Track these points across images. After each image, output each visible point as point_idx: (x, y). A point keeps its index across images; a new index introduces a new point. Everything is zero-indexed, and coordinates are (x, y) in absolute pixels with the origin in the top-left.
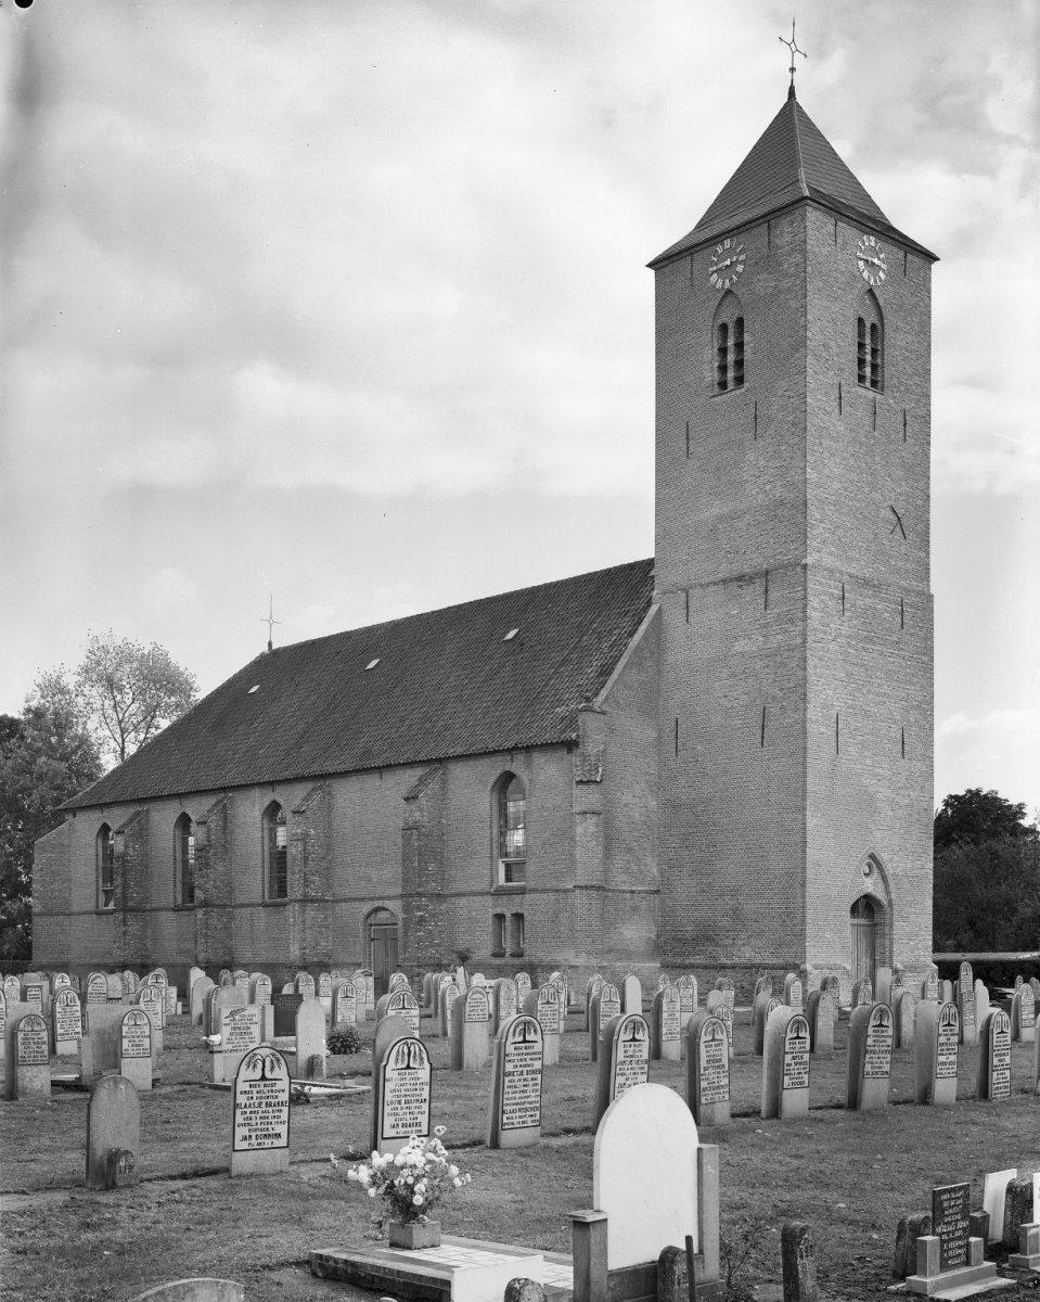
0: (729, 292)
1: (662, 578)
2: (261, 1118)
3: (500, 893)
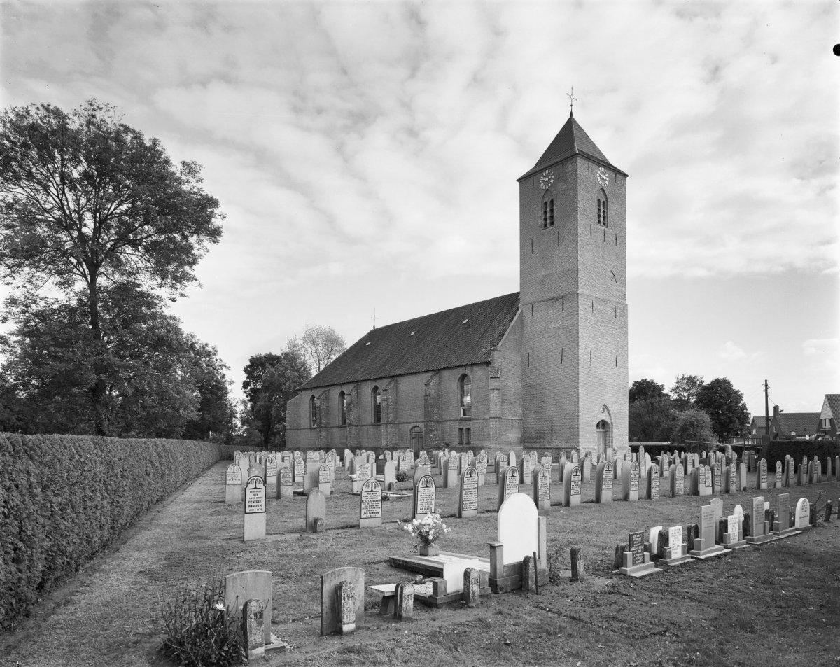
1: (523, 299)
3: (462, 420)
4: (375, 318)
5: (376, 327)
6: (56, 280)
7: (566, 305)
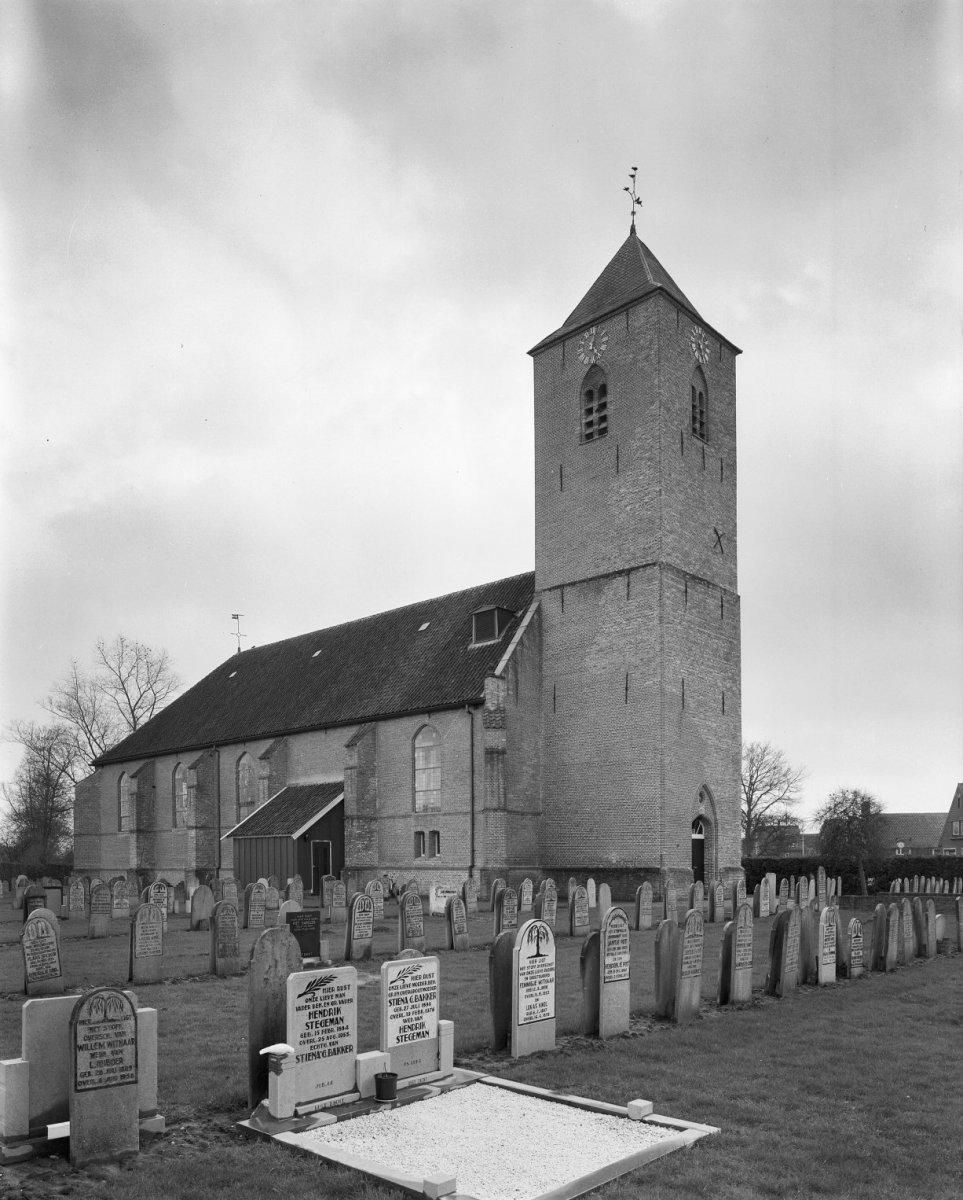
0: (594, 365)
2: (337, 995)
4: (239, 635)
5: (242, 651)
6: (238, 960)
7: (636, 588)
